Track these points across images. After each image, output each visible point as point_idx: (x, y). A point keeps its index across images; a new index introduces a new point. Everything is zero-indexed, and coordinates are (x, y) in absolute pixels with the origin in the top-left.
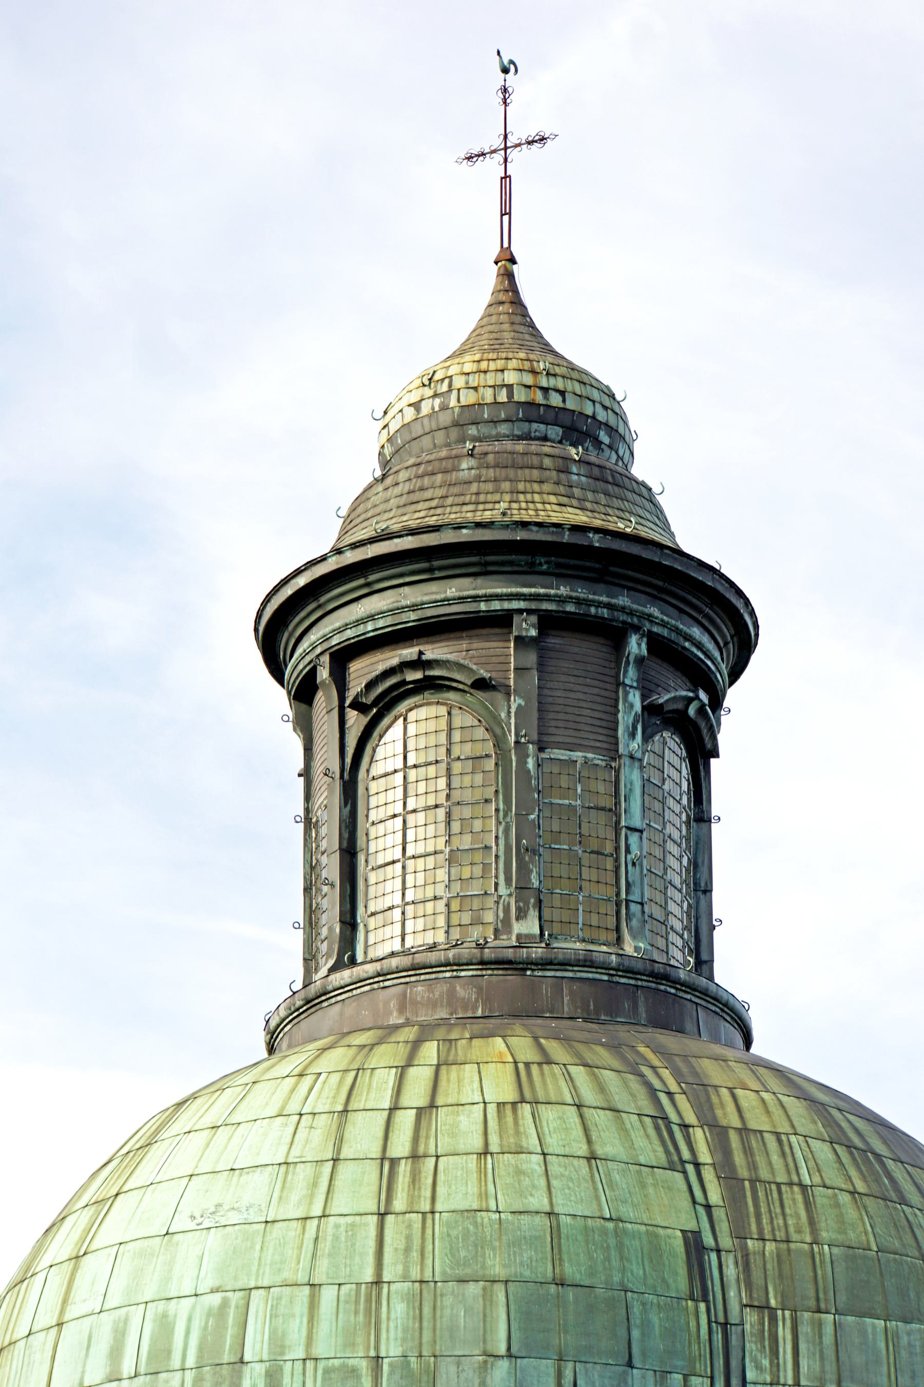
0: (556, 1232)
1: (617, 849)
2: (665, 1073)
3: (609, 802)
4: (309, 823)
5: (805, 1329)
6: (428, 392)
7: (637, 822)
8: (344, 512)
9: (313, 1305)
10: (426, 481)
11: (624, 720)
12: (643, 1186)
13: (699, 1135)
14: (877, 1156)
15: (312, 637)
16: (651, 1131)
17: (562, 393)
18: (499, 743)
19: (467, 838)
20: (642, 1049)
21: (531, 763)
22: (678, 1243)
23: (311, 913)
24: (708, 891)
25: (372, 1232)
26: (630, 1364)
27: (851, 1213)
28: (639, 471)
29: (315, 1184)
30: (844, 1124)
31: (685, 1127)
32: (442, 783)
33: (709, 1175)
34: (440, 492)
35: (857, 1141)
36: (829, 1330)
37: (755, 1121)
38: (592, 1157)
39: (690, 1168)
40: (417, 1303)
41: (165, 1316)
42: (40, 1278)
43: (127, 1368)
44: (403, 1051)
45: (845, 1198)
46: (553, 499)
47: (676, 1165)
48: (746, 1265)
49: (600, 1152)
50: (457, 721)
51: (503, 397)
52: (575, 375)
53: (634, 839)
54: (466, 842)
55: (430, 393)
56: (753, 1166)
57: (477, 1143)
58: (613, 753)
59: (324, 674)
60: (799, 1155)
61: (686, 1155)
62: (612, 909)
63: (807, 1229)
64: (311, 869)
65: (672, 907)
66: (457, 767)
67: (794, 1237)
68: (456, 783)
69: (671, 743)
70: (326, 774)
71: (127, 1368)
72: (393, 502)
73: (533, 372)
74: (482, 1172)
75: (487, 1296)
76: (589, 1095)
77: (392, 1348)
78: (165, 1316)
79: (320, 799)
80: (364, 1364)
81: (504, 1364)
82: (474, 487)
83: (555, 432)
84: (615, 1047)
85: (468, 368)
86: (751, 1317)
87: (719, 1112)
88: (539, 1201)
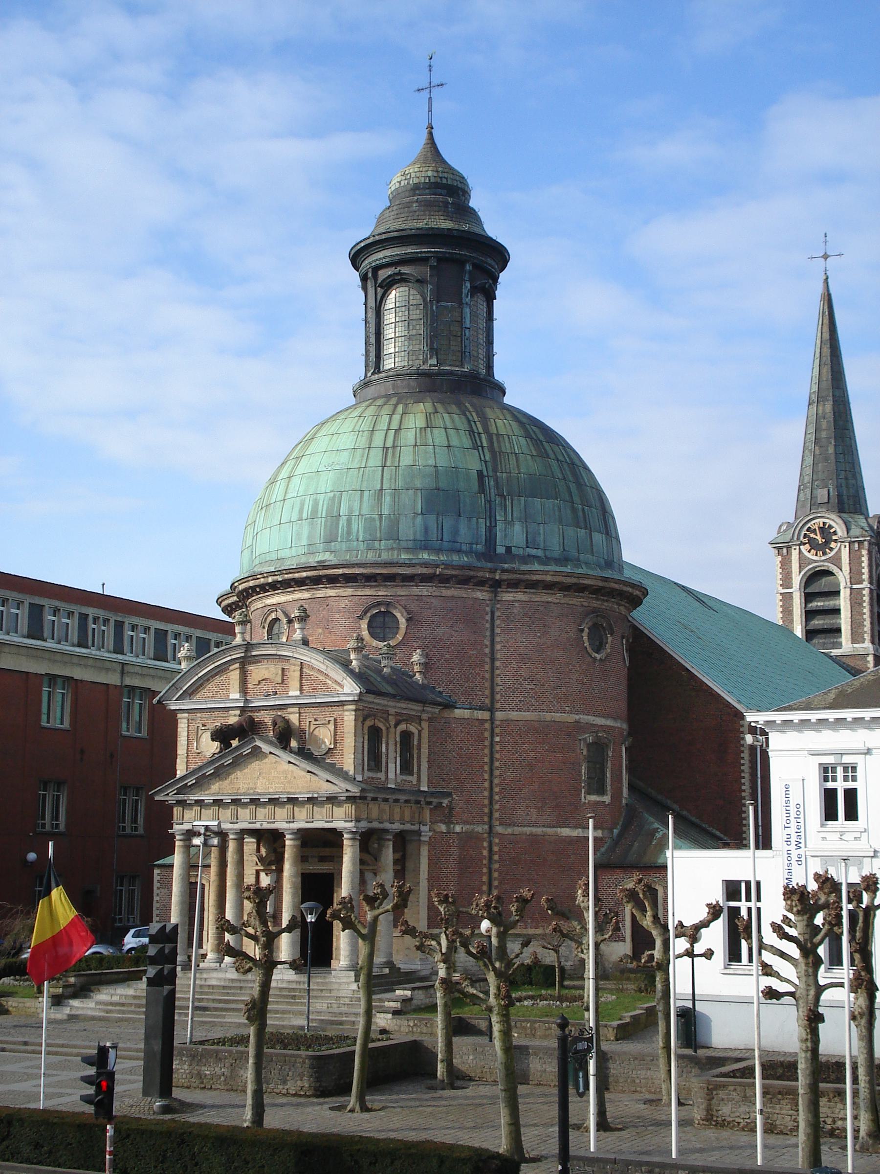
0: (437, 471)
1: (462, 334)
2: (474, 414)
3: (459, 319)
4: (366, 322)
5: (515, 502)
6: (404, 178)
7: (468, 326)
8: (377, 217)
9: (362, 496)
10: (402, 210)
11: (465, 291)
12: (465, 455)
13: (483, 436)
14: (541, 441)
15: (366, 262)
16: (468, 436)
17: (447, 179)
18: (425, 300)
19: (414, 331)
20: (467, 405)
21: (434, 308)
22: (475, 474)
23: (367, 351)
24: (492, 343)
25: (380, 473)
26: (460, 516)
27: (530, 462)
28: (472, 204)
29: (363, 456)
30: (531, 431)
31: (479, 434)
32: (407, 313)
33: (486, 450)
34: (407, 215)
35: (534, 437)
36: (523, 502)
37: (502, 431)
38: (449, 446)
39: (480, 448)
40: (393, 496)
41: (316, 500)
42: (279, 482)
43: (305, 516)
44: (392, 407)
45: (529, 457)
46: (442, 217)
47: (475, 447)
48: (496, 481)
49: (451, 444)
50: (412, 293)
51: (427, 181)
52: (451, 171)
53: (467, 331)
54: (414, 332)
55: (404, 178)
56: (500, 447)
57: (413, 443)
58: (461, 303)
59: (370, 275)
60: (515, 443)
61: (479, 444)
62: (460, 355)
63: (516, 469)
64: (367, 337)
65: (480, 351)
66: (411, 307)
67: (512, 471)
68: (411, 312)
69: (480, 297)
70: (276, 693)
71: (305, 516)
72: (392, 217)
73: (437, 171)
74: (414, 452)
75: (415, 493)
76: (449, 424)
77: (386, 512)
78: (316, 500)
79: (369, 315)
80: (377, 516)
81: (420, 516)
82: (417, 214)
83: (444, 192)
84: (459, 404)
85: (416, 170)
86: (498, 499)
87: (490, 428)
88: (431, 462)
